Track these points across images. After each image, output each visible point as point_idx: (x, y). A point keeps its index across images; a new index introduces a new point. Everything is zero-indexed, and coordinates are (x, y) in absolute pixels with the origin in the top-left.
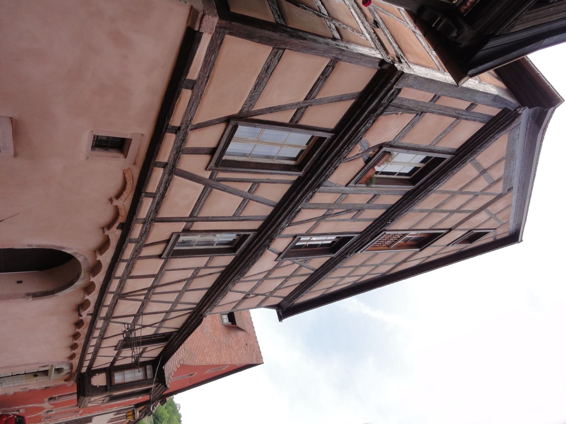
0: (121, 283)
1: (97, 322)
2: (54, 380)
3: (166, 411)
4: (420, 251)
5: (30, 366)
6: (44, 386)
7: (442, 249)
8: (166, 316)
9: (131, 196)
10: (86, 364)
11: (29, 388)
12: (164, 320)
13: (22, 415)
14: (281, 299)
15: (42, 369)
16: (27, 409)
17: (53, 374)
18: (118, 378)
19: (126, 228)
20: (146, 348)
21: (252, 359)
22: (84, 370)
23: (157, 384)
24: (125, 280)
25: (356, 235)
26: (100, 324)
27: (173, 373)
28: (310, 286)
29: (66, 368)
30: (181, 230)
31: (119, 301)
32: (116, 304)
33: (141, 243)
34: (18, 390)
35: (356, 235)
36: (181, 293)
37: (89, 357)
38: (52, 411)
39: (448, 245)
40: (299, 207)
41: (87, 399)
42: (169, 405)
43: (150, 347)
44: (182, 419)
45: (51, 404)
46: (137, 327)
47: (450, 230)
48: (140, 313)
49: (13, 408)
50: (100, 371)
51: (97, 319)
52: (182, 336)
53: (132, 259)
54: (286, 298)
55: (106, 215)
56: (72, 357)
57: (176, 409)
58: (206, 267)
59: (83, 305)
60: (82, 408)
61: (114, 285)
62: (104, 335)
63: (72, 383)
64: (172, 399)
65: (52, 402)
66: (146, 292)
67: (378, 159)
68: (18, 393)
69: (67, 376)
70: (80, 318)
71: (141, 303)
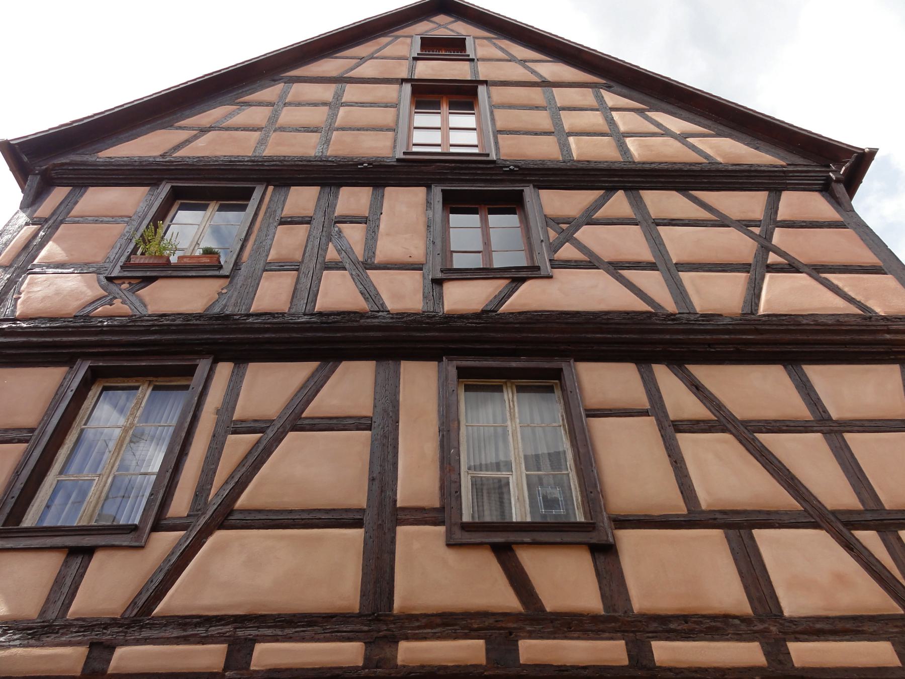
28: (709, 171)
67: (190, 274)
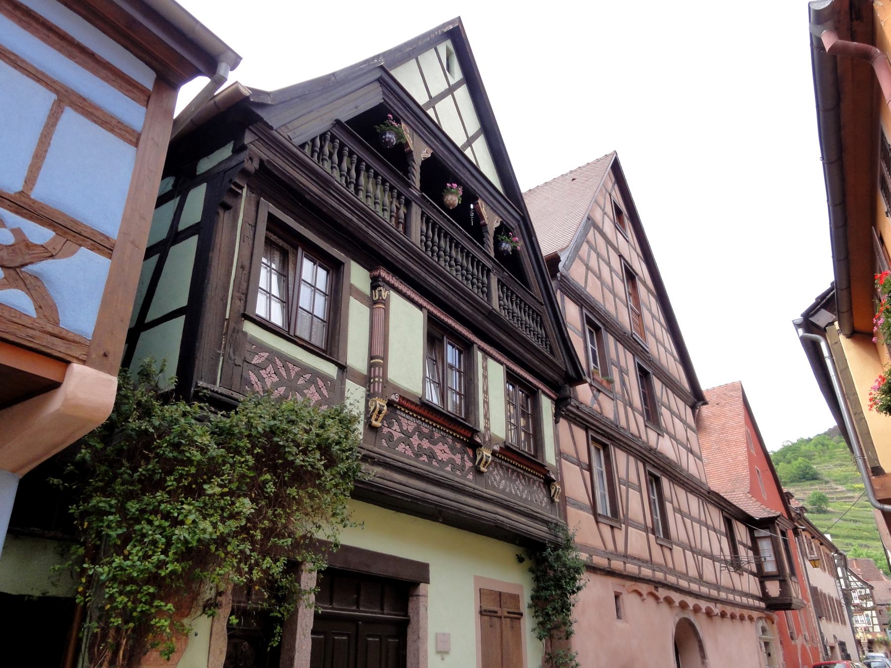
0: (692, 582)
1: (644, 576)
2: (773, 636)
3: (794, 462)
5: (762, 661)
6: (779, 645)
7: (631, 245)
8: (703, 525)
9: (640, 584)
11: (782, 661)
12: (715, 530)
14: (687, 406)
15: (764, 648)
17: (767, 637)
18: (770, 567)
19: (658, 584)
20: (738, 541)
21: (736, 397)
22: (763, 605)
23: (776, 524)
24: (690, 577)
26: (723, 595)
27: (762, 506)
29: (761, 624)
30: (653, 536)
31: (704, 580)
32: (707, 583)
36: (693, 519)
38: (805, 635)
39: (628, 242)
40: (630, 436)
41: (794, 601)
42: (784, 457)
43: (738, 537)
44: (806, 438)
45: (798, 636)
47: (621, 256)
48: (712, 558)
50: (763, 588)
51: (719, 598)
52: (727, 506)
53: (676, 576)
54: (686, 402)
56: (751, 619)
57: (791, 446)
58: (672, 502)
59: (709, 614)
60: (316, 137)
62: (731, 589)
64: (775, 453)
65: (795, 636)
66: (695, 555)
70: (719, 614)
71: (704, 558)
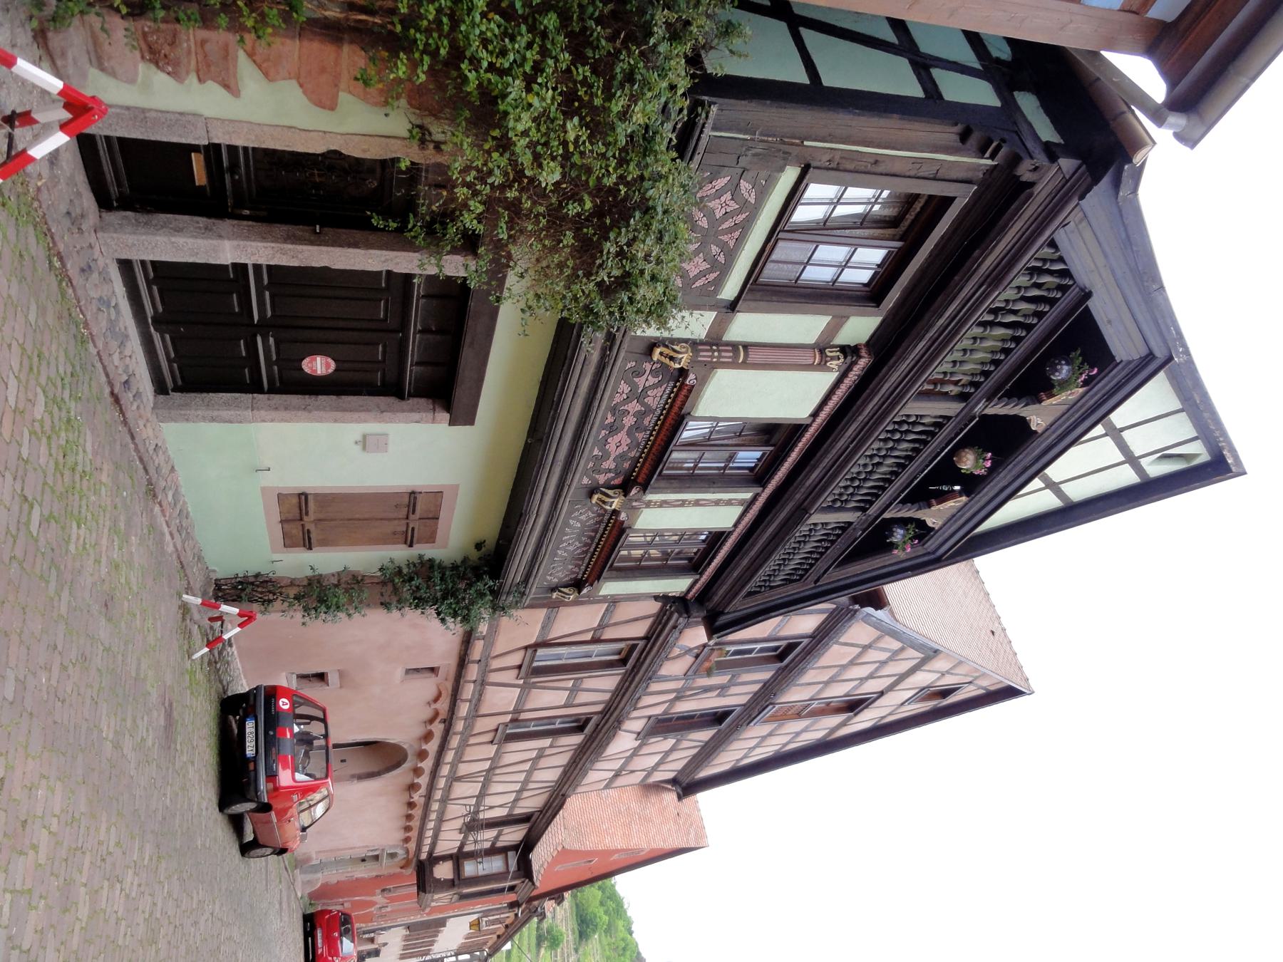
2: (386, 867)
4: (856, 715)
6: (374, 874)
9: (448, 701)
10: (426, 849)
13: (347, 911)
16: (353, 903)
17: (385, 860)
18: (469, 869)
19: (449, 723)
22: (424, 856)
25: (738, 708)
29: (401, 852)
33: (468, 733)
34: (343, 878)
35: (738, 708)
37: (428, 841)
39: (902, 704)
41: (428, 896)
43: (507, 830)
46: (482, 808)
49: (335, 900)
53: (459, 747)
54: (681, 772)
55: (427, 713)
56: (407, 840)
58: (551, 746)
59: (412, 787)
61: (445, 770)
63: (411, 872)
65: (387, 895)
68: (343, 882)
69: (404, 862)
